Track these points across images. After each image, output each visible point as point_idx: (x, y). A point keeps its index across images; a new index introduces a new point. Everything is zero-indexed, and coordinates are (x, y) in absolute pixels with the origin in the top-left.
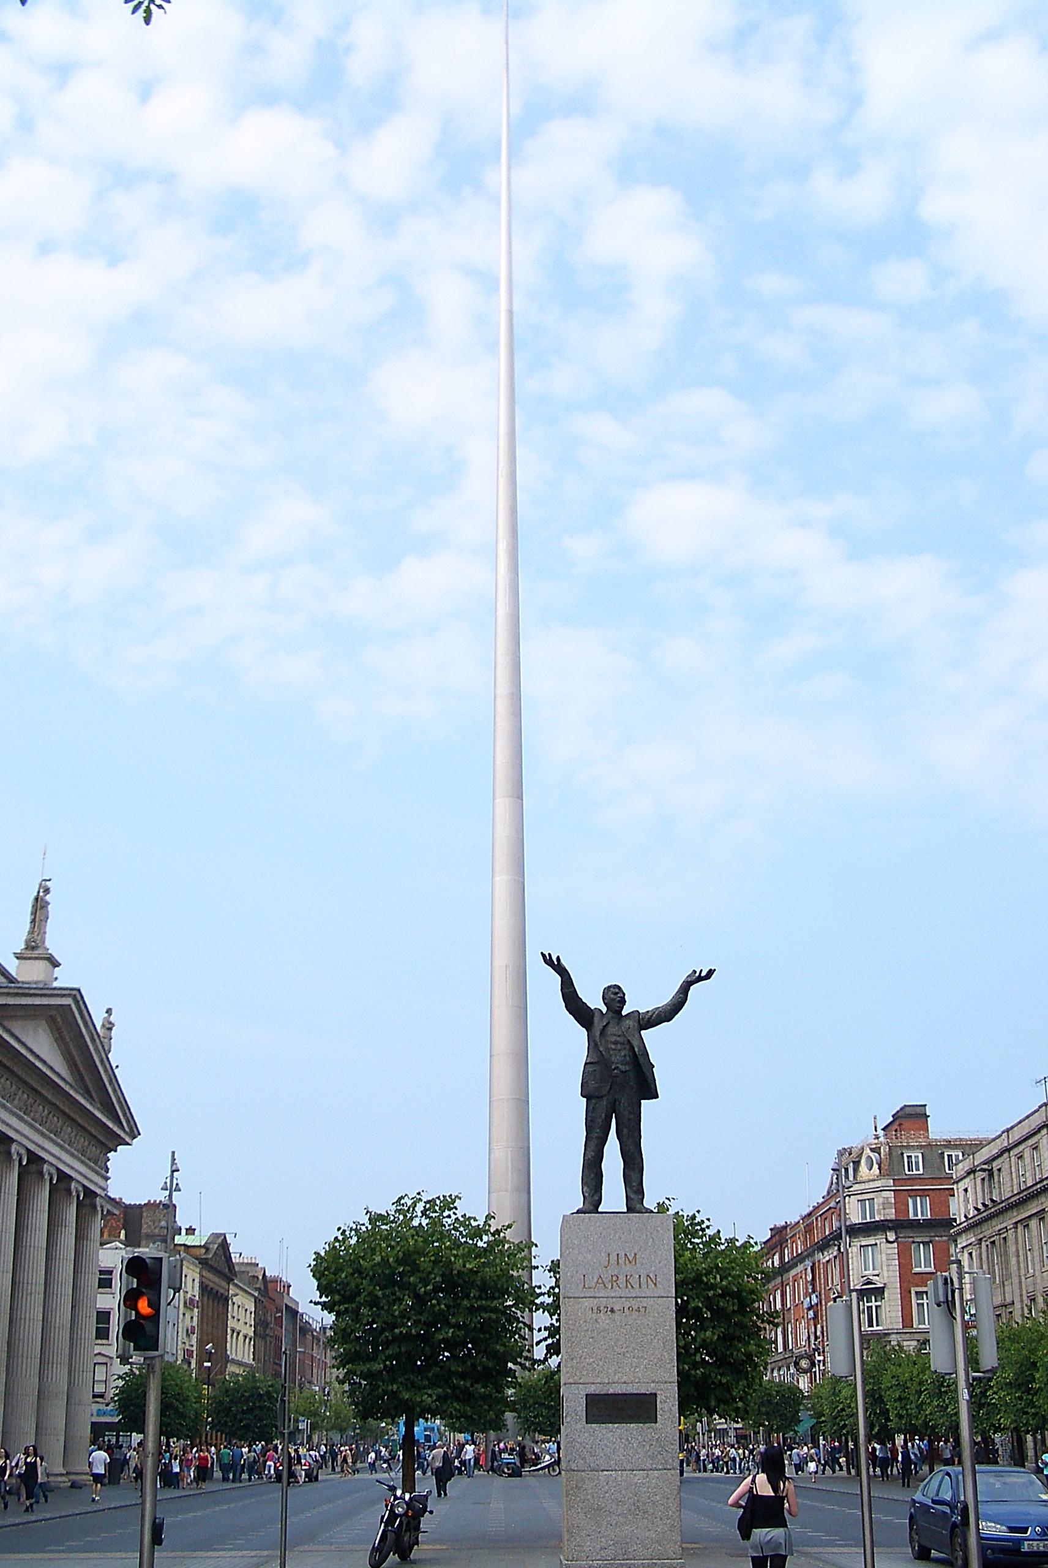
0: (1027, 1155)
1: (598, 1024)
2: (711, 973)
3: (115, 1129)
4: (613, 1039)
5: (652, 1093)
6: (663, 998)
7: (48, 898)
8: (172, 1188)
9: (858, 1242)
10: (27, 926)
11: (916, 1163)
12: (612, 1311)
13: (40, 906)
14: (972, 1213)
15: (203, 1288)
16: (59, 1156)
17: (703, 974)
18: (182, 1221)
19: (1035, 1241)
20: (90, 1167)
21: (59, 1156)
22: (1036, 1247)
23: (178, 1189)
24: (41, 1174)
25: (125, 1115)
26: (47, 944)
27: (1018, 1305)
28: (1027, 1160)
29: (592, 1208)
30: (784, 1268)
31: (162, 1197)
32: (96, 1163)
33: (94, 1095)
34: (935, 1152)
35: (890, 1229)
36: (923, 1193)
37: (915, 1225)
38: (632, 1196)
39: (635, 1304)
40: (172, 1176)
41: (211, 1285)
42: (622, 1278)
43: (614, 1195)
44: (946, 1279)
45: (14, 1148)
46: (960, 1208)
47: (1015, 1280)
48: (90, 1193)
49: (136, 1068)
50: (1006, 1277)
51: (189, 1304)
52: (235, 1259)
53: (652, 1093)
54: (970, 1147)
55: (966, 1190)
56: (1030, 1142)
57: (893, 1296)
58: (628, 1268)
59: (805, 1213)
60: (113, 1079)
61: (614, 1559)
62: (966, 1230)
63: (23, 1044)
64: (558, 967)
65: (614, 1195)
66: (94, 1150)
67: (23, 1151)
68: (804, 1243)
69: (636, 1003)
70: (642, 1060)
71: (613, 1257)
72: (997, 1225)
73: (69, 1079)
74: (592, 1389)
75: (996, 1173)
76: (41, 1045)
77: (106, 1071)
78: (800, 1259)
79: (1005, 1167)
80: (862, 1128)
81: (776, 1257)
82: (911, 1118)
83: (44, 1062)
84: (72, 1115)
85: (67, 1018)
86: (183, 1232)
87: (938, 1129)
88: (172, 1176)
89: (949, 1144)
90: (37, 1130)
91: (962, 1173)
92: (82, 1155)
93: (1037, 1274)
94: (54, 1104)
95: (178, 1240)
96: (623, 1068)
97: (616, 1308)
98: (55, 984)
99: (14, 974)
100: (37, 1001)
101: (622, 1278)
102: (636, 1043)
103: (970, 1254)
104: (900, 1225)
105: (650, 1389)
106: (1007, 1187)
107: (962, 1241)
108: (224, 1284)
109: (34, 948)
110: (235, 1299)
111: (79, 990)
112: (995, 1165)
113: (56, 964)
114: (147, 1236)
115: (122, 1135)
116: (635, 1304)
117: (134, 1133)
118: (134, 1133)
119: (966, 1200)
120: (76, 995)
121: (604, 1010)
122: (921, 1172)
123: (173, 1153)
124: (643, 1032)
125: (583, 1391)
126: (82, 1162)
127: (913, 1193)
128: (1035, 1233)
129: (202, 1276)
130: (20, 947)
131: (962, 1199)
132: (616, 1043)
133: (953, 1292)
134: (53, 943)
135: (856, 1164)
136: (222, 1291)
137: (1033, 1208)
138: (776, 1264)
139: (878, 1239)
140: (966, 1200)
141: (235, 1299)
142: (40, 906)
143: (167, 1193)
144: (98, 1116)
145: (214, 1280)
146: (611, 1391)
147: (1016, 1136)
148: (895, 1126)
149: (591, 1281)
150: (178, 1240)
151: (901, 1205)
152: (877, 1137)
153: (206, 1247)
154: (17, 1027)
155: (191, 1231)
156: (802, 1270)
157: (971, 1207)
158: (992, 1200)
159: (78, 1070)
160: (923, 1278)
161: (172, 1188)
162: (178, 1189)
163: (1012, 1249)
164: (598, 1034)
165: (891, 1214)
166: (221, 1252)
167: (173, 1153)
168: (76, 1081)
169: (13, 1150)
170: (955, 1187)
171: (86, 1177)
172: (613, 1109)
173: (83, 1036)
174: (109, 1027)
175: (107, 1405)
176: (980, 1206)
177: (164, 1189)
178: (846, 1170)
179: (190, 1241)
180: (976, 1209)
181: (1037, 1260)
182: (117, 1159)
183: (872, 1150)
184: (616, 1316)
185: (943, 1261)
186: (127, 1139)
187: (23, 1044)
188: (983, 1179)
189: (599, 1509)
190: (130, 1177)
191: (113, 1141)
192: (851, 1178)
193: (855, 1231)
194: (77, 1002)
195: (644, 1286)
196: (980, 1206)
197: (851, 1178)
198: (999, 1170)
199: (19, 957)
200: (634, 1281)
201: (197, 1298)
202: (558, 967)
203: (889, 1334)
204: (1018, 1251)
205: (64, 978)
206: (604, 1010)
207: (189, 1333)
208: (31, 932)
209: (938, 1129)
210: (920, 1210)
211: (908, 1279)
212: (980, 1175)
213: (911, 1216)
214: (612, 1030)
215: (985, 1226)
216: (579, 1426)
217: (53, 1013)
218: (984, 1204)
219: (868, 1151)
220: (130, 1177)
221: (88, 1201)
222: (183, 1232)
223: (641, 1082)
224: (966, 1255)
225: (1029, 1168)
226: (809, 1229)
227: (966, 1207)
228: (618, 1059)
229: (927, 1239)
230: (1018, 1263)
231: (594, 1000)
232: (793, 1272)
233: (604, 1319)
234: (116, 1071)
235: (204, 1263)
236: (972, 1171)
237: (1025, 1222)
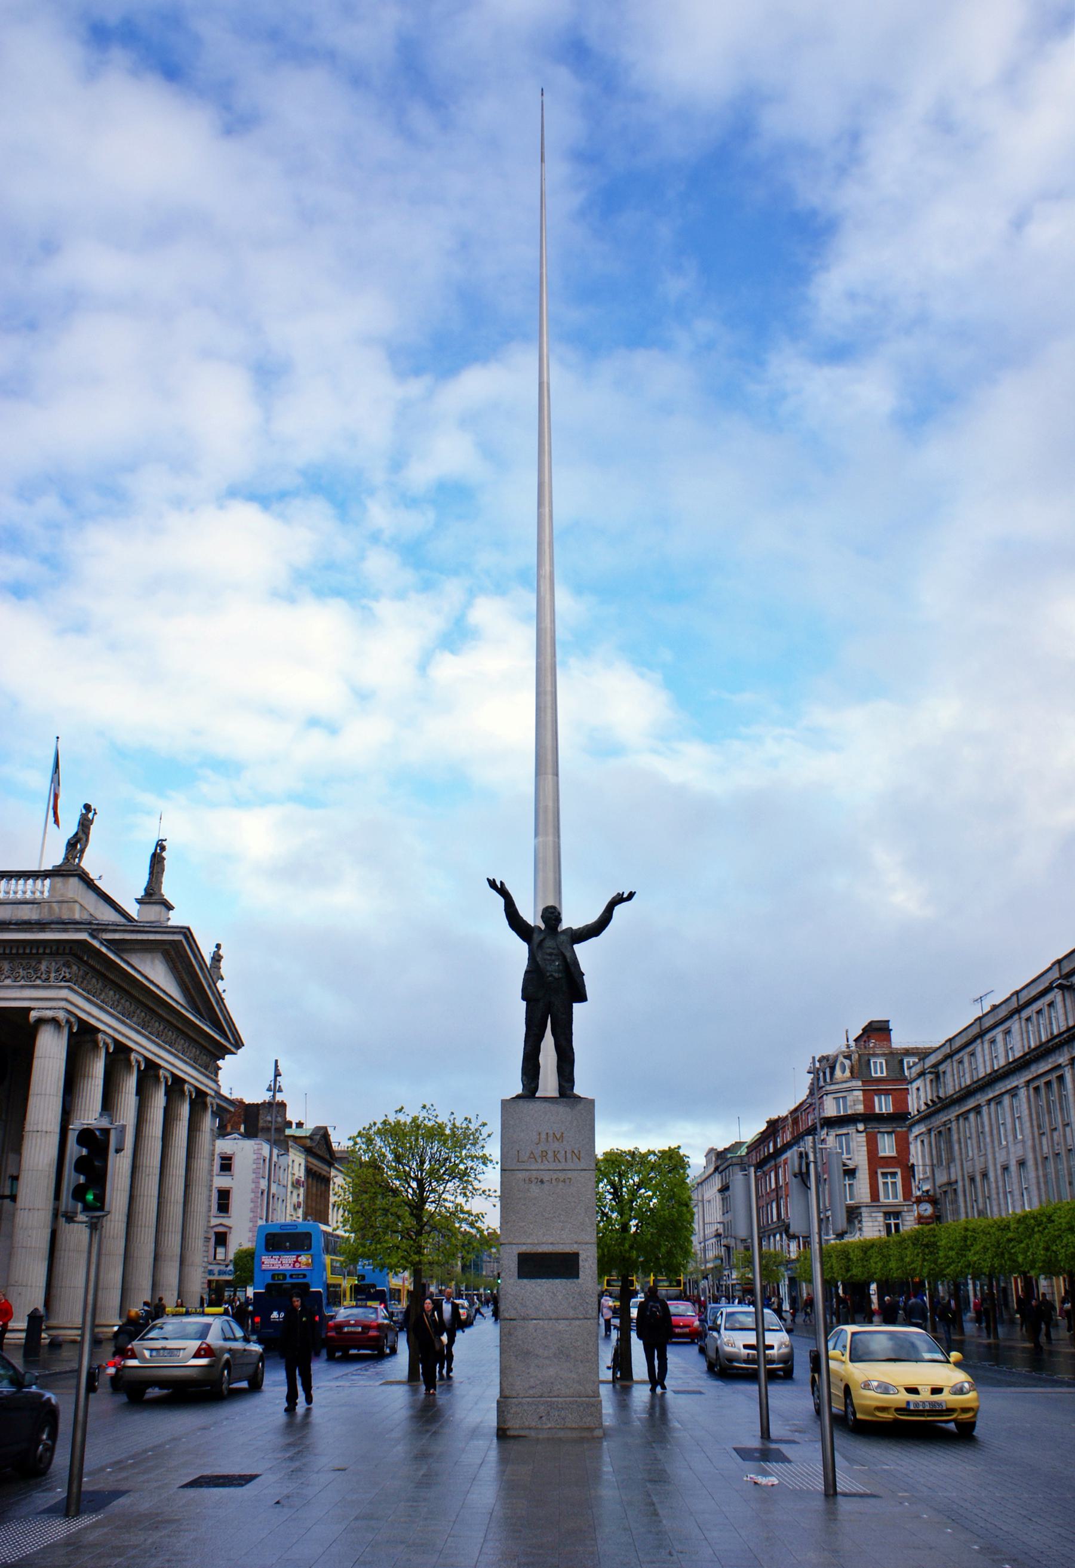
0: (966, 1060)
1: (537, 938)
2: (631, 895)
3: (222, 1041)
4: (549, 951)
5: (583, 998)
6: (592, 917)
7: (164, 854)
8: (275, 1089)
9: (833, 1133)
10: (146, 877)
11: (879, 1069)
12: (542, 1182)
13: (157, 862)
14: (923, 1107)
15: (309, 1171)
16: (173, 1062)
17: (625, 896)
18: (292, 1116)
19: (973, 1130)
20: (201, 1073)
21: (173, 1062)
22: (974, 1135)
23: (280, 1090)
24: (157, 1077)
25: (230, 1030)
26: (163, 891)
27: (960, 1184)
28: (966, 1064)
29: (528, 1093)
30: (779, 1152)
31: (266, 1097)
32: (206, 1068)
33: (205, 1015)
34: (896, 1058)
35: (860, 1121)
36: (887, 1092)
37: (881, 1118)
38: (564, 1084)
39: (561, 1176)
40: (275, 1080)
41: (315, 1169)
42: (550, 1154)
43: (548, 1082)
44: (801, 1153)
45: (133, 1056)
46: (915, 1103)
47: (958, 1162)
48: (201, 1094)
49: (235, 994)
50: (951, 1160)
51: (296, 1184)
52: (335, 1147)
53: (581, 996)
54: (923, 1054)
55: (918, 1089)
56: (969, 1049)
57: (863, 1175)
58: (556, 1145)
59: (792, 1108)
60: (220, 1000)
61: (541, 1397)
62: (918, 1122)
63: (139, 972)
64: (502, 891)
65: (548, 1082)
66: (205, 1058)
67: (141, 1059)
68: (792, 1133)
69: (572, 919)
70: (573, 968)
71: (543, 1136)
72: (942, 1118)
73: (181, 1000)
74: (524, 1249)
75: (941, 1075)
76: (157, 974)
77: (213, 993)
78: (787, 1146)
79: (949, 1070)
80: (837, 1038)
81: (771, 1145)
82: (878, 1030)
83: (158, 987)
84: (186, 1030)
85: (179, 950)
86: (294, 1126)
87: (899, 1039)
88: (275, 1080)
89: (908, 1052)
90: (154, 1042)
91: (913, 1075)
92: (195, 1062)
93: (976, 1157)
94: (168, 1021)
95: (288, 1132)
96: (556, 975)
97: (545, 1179)
98: (170, 923)
99: (136, 918)
100: (152, 937)
101: (550, 1154)
102: (568, 955)
103: (922, 1141)
104: (869, 1118)
105: (574, 1248)
106: (950, 1087)
107: (917, 1130)
108: (326, 1168)
109: (152, 895)
110: (335, 1180)
111: (188, 929)
112: (942, 1068)
113: (170, 908)
114: (263, 1129)
115: (229, 1046)
116: (561, 1176)
117: (239, 1044)
118: (239, 1044)
119: (919, 1098)
120: (186, 932)
121: (543, 926)
122: (885, 1074)
123: (276, 1061)
124: (576, 947)
125: (516, 1250)
126: (195, 1068)
127: (879, 1092)
128: (973, 1124)
129: (307, 1161)
130: (140, 893)
131: (915, 1096)
132: (551, 954)
133: (808, 1165)
134: (168, 890)
135: (833, 1069)
136: (324, 1173)
137: (971, 1104)
138: (771, 1151)
139: (850, 1129)
140: (919, 1098)
141: (335, 1180)
142: (157, 862)
143: (271, 1093)
144: (209, 1033)
145: (318, 1165)
146: (540, 1250)
147: (957, 1044)
148: (864, 1038)
149: (524, 1156)
150: (288, 1132)
151: (868, 1103)
152: (848, 1047)
153: (310, 1138)
154: (135, 960)
155: (300, 1125)
156: (791, 1154)
157: (922, 1102)
158: (938, 1097)
159: (190, 994)
160: (887, 1161)
161: (275, 1089)
162: (280, 1090)
163: (955, 1137)
164: (535, 946)
165: (860, 1108)
166: (323, 1142)
167: (276, 1061)
168: (188, 1003)
169: (132, 1058)
170: (909, 1087)
171: (197, 1080)
172: (548, 1010)
173: (193, 966)
174: (217, 958)
175: (227, 1266)
176: (930, 1103)
177: (269, 1090)
178: (824, 1073)
179: (299, 1133)
180: (926, 1104)
181: (975, 1145)
182: (227, 1064)
183: (846, 1057)
184: (546, 1186)
185: (903, 1147)
186: (233, 1049)
187: (139, 972)
188: (918, 1089)
189: (528, 1353)
190: (239, 1079)
191: (222, 1052)
192: (828, 1080)
193: (830, 1123)
194: (187, 938)
195: (569, 1161)
196: (930, 1103)
197: (828, 1080)
198: (944, 1072)
199: (140, 901)
200: (561, 1156)
201: (303, 1179)
202: (502, 891)
203: (859, 1207)
204: (959, 1139)
205: (175, 919)
206: (543, 926)
207: (296, 1207)
208: (150, 882)
209: (899, 1039)
210: (884, 1105)
211: (875, 1161)
212: (929, 1077)
213: (877, 1111)
214: (549, 943)
215: (933, 1119)
216: (512, 1281)
217: (167, 947)
218: (932, 1101)
219: (841, 1058)
220: (239, 1079)
221: (199, 1100)
222: (294, 1126)
223: (574, 988)
224: (919, 1143)
225: (967, 1071)
226: (795, 1122)
227: (918, 1103)
228: (554, 968)
229: (889, 1130)
230: (960, 1149)
231: (530, 915)
232: (784, 1157)
233: (535, 1190)
234: (223, 995)
235: (309, 1151)
236: (922, 1074)
237: (965, 1116)
